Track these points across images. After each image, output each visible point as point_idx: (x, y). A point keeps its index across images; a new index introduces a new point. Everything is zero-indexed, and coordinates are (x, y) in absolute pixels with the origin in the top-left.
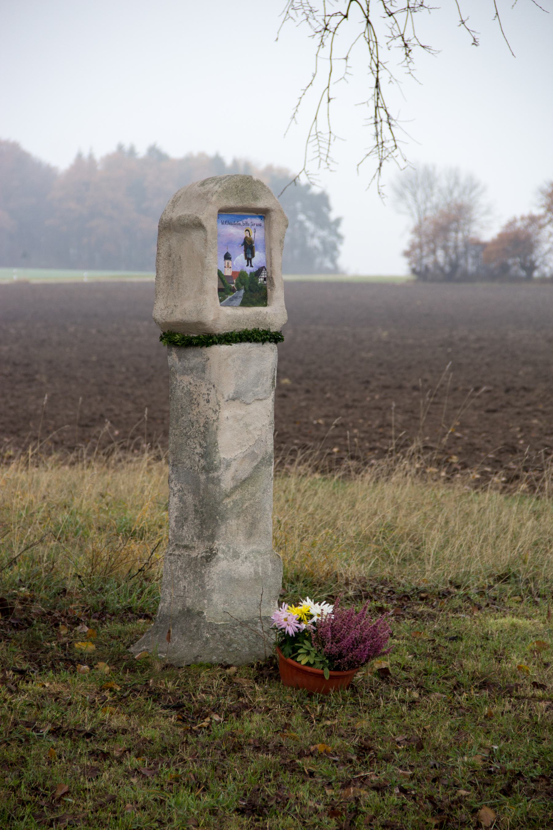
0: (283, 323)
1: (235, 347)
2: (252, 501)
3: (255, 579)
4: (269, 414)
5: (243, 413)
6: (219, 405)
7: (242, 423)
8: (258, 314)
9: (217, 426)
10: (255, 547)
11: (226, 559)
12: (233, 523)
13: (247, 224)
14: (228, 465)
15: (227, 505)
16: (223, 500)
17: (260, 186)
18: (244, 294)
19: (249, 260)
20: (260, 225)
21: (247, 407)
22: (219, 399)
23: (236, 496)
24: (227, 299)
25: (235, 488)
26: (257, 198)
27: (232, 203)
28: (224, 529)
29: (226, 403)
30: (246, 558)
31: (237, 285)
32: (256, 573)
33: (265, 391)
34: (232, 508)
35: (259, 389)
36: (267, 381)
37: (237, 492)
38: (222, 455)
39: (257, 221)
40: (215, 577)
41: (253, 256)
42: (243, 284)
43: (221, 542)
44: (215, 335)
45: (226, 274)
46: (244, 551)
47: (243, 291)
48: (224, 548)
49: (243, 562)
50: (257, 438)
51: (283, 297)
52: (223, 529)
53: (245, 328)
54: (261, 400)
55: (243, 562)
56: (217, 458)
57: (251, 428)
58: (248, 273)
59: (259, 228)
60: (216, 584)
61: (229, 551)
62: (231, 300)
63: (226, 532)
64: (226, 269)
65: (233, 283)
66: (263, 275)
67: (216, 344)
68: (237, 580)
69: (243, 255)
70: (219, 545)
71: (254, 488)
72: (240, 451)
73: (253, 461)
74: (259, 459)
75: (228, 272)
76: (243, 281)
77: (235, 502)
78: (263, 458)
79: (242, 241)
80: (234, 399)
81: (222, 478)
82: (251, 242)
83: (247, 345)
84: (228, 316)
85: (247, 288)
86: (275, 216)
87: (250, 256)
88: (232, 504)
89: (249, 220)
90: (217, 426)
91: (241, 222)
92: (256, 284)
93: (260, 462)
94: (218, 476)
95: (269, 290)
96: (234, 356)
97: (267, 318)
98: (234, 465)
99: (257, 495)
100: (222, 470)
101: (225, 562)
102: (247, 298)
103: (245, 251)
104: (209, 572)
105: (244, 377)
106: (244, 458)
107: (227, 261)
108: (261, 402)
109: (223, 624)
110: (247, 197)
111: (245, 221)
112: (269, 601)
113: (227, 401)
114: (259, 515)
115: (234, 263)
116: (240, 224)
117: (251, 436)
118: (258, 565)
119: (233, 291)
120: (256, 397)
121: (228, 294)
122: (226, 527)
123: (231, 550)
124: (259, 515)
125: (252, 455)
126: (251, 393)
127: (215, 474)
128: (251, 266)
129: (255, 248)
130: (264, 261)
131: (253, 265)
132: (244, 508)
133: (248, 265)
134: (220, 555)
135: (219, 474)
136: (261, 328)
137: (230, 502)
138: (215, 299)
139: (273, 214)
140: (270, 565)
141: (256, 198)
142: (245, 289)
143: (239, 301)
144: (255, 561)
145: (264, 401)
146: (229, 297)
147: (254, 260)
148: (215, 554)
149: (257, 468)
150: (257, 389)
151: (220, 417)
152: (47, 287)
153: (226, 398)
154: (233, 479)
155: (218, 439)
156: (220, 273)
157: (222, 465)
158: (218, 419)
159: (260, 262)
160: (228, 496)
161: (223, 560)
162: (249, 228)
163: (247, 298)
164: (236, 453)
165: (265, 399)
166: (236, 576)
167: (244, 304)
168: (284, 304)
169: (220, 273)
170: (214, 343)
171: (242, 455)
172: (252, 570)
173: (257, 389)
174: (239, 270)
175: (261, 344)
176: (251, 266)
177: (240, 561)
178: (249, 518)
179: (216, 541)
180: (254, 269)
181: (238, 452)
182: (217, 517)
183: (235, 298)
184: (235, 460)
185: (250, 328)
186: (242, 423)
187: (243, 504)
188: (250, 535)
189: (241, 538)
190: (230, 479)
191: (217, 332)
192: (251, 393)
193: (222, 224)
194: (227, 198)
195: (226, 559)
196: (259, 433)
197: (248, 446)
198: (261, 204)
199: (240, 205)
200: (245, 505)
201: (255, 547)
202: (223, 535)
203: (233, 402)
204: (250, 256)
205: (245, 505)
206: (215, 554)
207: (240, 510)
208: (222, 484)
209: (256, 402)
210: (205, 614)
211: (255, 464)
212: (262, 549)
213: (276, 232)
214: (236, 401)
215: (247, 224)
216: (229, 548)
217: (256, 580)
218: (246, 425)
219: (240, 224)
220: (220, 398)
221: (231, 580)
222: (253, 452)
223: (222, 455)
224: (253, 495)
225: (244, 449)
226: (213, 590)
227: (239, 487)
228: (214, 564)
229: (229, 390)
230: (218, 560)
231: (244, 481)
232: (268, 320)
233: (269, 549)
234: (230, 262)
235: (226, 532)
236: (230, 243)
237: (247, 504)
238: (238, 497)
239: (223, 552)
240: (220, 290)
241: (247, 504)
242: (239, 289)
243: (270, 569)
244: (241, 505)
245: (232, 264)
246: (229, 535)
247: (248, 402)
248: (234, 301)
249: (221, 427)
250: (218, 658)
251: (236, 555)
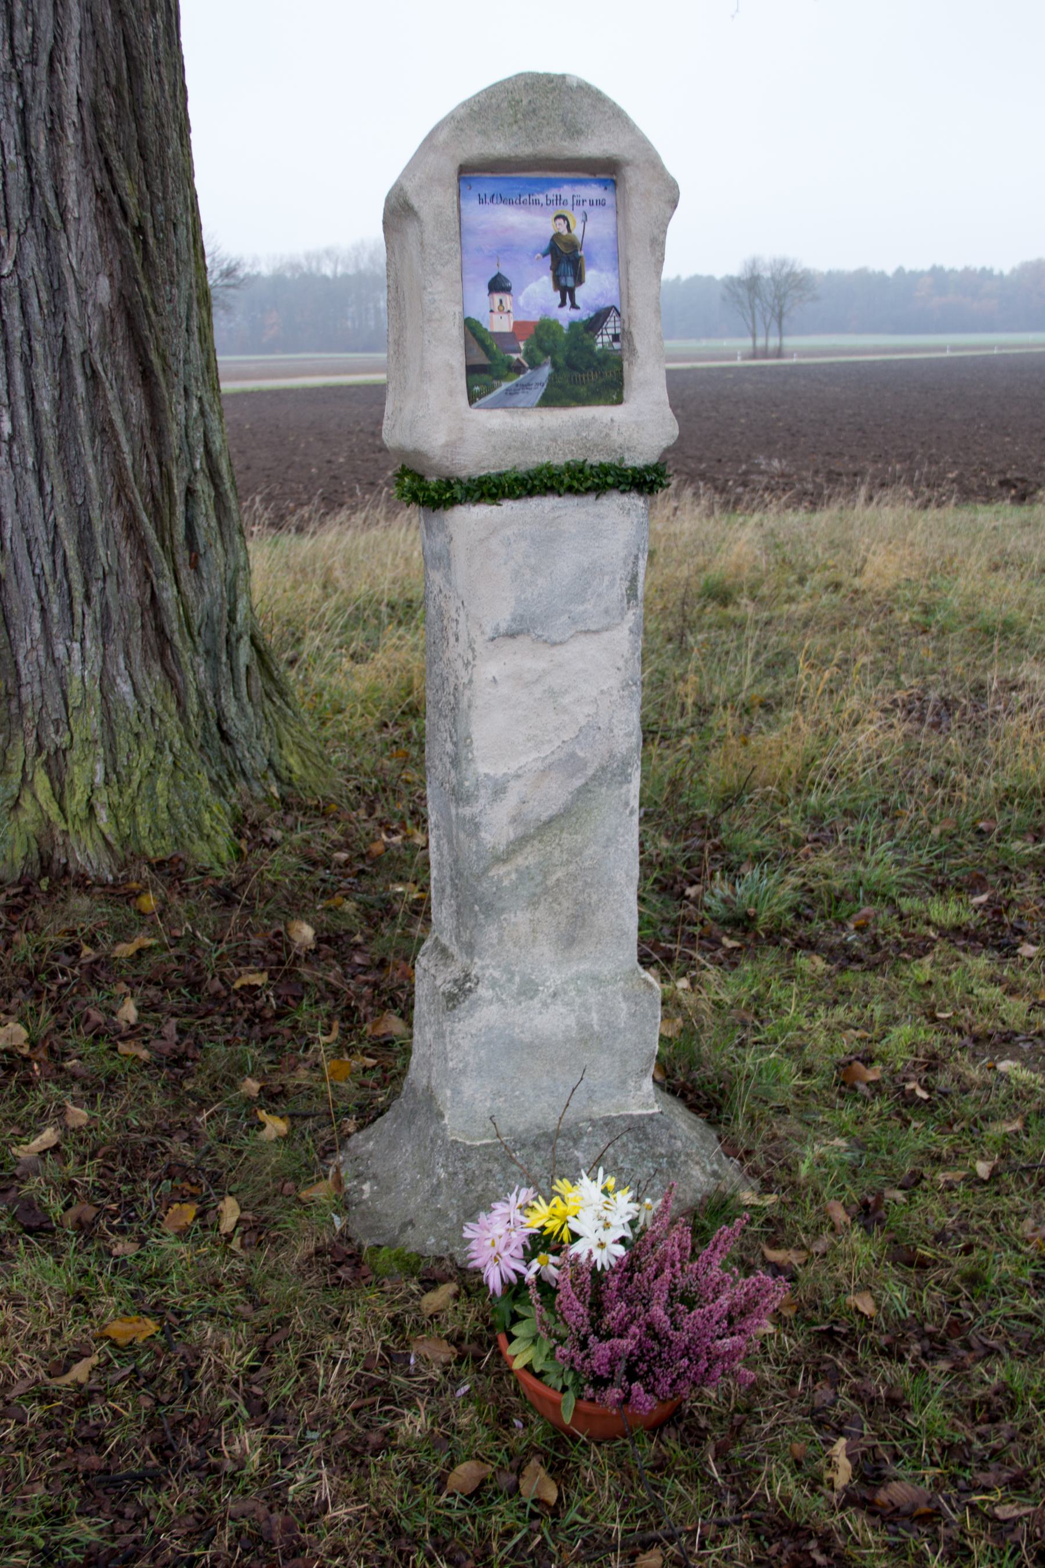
0: (664, 444)
1: (509, 507)
2: (572, 868)
3: (582, 1040)
4: (621, 663)
5: (542, 665)
6: (473, 650)
7: (538, 690)
8: (587, 425)
9: (470, 701)
10: (584, 966)
11: (500, 1000)
12: (519, 919)
13: (559, 199)
14: (499, 790)
15: (500, 881)
16: (487, 869)
17: (587, 101)
18: (552, 379)
19: (566, 293)
20: (601, 203)
21: (554, 651)
22: (473, 635)
23: (527, 859)
24: (498, 391)
25: (521, 842)
26: (580, 132)
27: (500, 147)
28: (495, 934)
29: (491, 646)
30: (555, 995)
31: (528, 354)
32: (583, 1027)
33: (606, 611)
34: (515, 887)
35: (588, 606)
36: (612, 583)
37: (529, 849)
38: (483, 768)
39: (593, 192)
40: (466, 1044)
41: (579, 280)
42: (547, 353)
43: (488, 961)
44: (459, 481)
45: (496, 329)
46: (555, 978)
47: (547, 370)
48: (497, 974)
49: (545, 1005)
50: (583, 722)
51: (664, 382)
52: (492, 933)
53: (545, 459)
54: (596, 632)
55: (545, 1005)
56: (469, 774)
57: (566, 700)
58: (565, 324)
59: (596, 210)
60: (470, 1059)
61: (510, 980)
62: (509, 392)
63: (501, 940)
64: (496, 317)
65: (518, 351)
66: (611, 327)
67: (461, 503)
68: (531, 1045)
69: (547, 279)
70: (482, 968)
71: (579, 838)
72: (534, 755)
73: (572, 776)
74: (590, 772)
75: (501, 324)
76: (547, 345)
77: (524, 874)
78: (603, 769)
79: (546, 245)
80: (512, 635)
81: (484, 820)
82: (574, 246)
83: (549, 502)
84: (492, 432)
85: (561, 361)
86: (633, 177)
87: (570, 282)
88: (514, 876)
89: (566, 192)
90: (470, 701)
91: (542, 198)
92: (590, 350)
93: (594, 778)
94: (473, 817)
95: (625, 364)
96: (508, 532)
97: (614, 435)
98: (515, 791)
99: (588, 852)
100: (482, 801)
101: (494, 1008)
102: (561, 387)
103: (555, 269)
104: (452, 1033)
105: (540, 581)
106: (544, 772)
107: (497, 297)
108: (595, 637)
109: (487, 1146)
110: (546, 130)
111: (552, 193)
112: (624, 1082)
113: (493, 639)
114: (595, 897)
115: (521, 300)
116: (537, 202)
117: (566, 718)
118: (588, 1010)
119: (518, 369)
120: (581, 627)
121: (500, 378)
122: (501, 928)
123: (517, 979)
124: (595, 897)
125: (571, 763)
126: (564, 618)
127: (466, 811)
128: (574, 306)
129: (585, 262)
130: (615, 293)
131: (578, 302)
132: (551, 881)
133: (563, 304)
134: (483, 992)
135: (476, 810)
136: (595, 459)
137: (509, 873)
138: (451, 393)
139: (629, 172)
140: (623, 1005)
141: (574, 132)
142: (554, 364)
143: (537, 393)
144: (578, 1001)
145: (606, 635)
146: (505, 385)
147: (580, 293)
148: (470, 990)
149: (583, 791)
150: (581, 608)
151: (475, 677)
152: (901, 360)
153: (489, 633)
154: (514, 820)
155: (473, 729)
156: (472, 329)
157: (483, 792)
158: (471, 681)
159: (601, 295)
160: (501, 859)
161: (491, 1002)
162: (566, 211)
163: (561, 387)
164: (523, 760)
165: (607, 629)
166: (527, 1037)
167: (550, 400)
168: (665, 397)
169: (472, 329)
170: (453, 502)
171: (539, 765)
172: (571, 1021)
173: (581, 608)
174: (535, 317)
175: (591, 498)
176: (574, 306)
177: (536, 1003)
178: (566, 904)
179: (476, 960)
180: (583, 314)
181: (529, 759)
182: (477, 908)
183: (525, 386)
184: (518, 776)
185: (559, 460)
186: (538, 690)
187: (546, 875)
188: (569, 941)
189: (545, 949)
190: (505, 820)
191: (463, 474)
192: (564, 618)
193: (481, 201)
194: (484, 133)
195: (500, 1000)
196: (590, 710)
197: (558, 743)
198: (590, 148)
199: (526, 150)
200: (554, 878)
201: (584, 966)
202: (491, 945)
203: (511, 641)
204: (570, 282)
205: (554, 878)
206: (470, 990)
207: (538, 890)
208: (483, 834)
209: (582, 638)
210: (446, 1121)
211: (578, 783)
212: (606, 969)
213: (639, 221)
214: (520, 638)
215: (559, 199)
216: (512, 974)
217: (584, 1041)
218: (553, 694)
219: (537, 202)
220: (475, 633)
221: (513, 1047)
222: (573, 755)
223: (483, 768)
224: (575, 853)
225: (547, 750)
226: (463, 1072)
227: (533, 837)
228: (463, 1014)
229: (502, 615)
230: (474, 1005)
231: (551, 821)
232: (616, 439)
233: (627, 968)
234: (507, 299)
235: (501, 940)
236: (507, 248)
237: (559, 874)
238: (531, 860)
239: (494, 984)
240: (472, 370)
241: (559, 874)
242: (535, 365)
243: (623, 1015)
244: (539, 878)
245: (515, 303)
246: (510, 945)
247: (556, 638)
248: (521, 395)
249: (478, 702)
250: (438, 1243)
251: (528, 990)
